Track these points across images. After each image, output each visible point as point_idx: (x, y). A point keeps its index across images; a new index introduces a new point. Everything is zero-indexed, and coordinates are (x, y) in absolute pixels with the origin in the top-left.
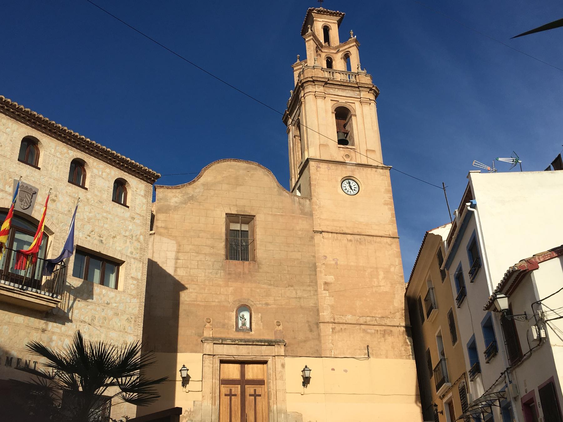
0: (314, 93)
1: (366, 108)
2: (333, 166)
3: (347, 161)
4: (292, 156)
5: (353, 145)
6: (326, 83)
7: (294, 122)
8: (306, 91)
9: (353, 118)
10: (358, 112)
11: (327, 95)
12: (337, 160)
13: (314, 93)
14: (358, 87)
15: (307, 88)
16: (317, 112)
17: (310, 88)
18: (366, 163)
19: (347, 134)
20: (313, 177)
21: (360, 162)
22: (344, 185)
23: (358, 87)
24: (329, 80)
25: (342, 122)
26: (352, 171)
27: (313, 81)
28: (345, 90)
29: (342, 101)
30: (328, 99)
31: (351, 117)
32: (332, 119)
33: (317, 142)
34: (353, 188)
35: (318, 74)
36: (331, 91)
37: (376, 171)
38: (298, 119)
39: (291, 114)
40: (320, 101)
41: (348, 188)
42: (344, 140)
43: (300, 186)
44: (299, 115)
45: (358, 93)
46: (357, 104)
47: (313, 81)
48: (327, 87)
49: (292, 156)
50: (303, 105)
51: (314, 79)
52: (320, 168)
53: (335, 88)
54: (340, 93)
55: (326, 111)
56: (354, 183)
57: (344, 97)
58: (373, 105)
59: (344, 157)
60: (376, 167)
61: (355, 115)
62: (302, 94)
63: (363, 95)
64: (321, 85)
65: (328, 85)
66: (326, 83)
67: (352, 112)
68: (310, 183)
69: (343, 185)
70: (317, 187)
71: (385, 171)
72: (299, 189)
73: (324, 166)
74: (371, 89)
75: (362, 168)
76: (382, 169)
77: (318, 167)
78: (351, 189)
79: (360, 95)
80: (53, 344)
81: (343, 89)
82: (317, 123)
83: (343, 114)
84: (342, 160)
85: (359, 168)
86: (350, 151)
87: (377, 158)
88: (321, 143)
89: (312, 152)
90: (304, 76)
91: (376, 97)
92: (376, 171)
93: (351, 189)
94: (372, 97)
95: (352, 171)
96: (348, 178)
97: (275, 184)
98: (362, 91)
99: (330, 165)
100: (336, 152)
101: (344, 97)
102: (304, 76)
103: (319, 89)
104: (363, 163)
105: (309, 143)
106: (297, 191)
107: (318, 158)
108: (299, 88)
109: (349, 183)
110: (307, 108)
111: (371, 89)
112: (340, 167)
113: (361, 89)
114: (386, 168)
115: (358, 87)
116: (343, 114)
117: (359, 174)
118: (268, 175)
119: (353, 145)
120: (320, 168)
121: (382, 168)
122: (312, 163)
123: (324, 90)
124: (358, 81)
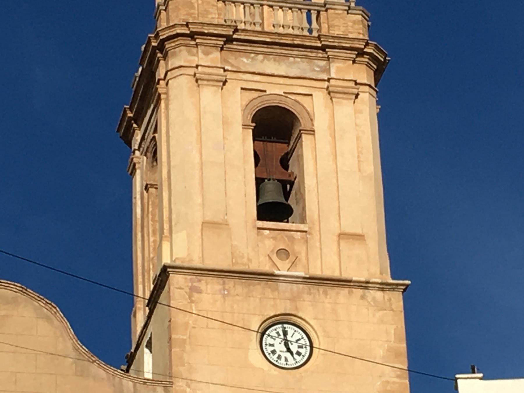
0: (191, 71)
1: (345, 108)
2: (237, 287)
3: (283, 268)
4: (139, 243)
5: (303, 220)
6: (229, 40)
7: (145, 145)
8: (173, 62)
9: (305, 138)
10: (320, 123)
11: (229, 75)
12: (254, 267)
13: (191, 71)
14: (323, 48)
15: (174, 54)
16: (200, 128)
17: (181, 56)
18: (336, 274)
19: (292, 184)
20: (179, 318)
21: (318, 273)
22: (270, 341)
23: (325, 48)
24: (236, 30)
25: (278, 149)
26: (293, 299)
27: (192, 36)
28: (287, 56)
29: (275, 91)
30: (234, 86)
31: (299, 137)
32: (242, 145)
33: (198, 217)
34: (294, 348)
35: (207, 12)
36: (245, 62)
37: (363, 297)
38: (154, 138)
39: (138, 119)
40: (209, 94)
41: (280, 347)
42: (277, 205)
43: (150, 338)
44: (155, 131)
45: (323, 63)
46: (319, 99)
47: (192, 36)
48: (231, 50)
49: (139, 243)
50: (163, 104)
51: (194, 28)
52: (200, 292)
53: (257, 53)
54: (270, 66)
55: (226, 123)
56: (299, 334)
57: (279, 79)
58: (367, 101)
59: (274, 257)
60: (365, 285)
61: (312, 132)
62: (161, 73)
63: (338, 70)
64: (215, 46)
65: (235, 46)
66: (229, 40)
67: (304, 123)
68: (170, 338)
69: (267, 340)
70: (188, 347)
71: (388, 294)
72: (149, 346)
73: (210, 287)
74: (361, 53)
75: (321, 289)
76: (382, 289)
77: (194, 290)
78: (289, 350)
79: (328, 71)
80: (232, 283)
81: (278, 55)
82: (197, 160)
83: (275, 129)
84: (266, 268)
85: (314, 289)
86: (292, 240)
87: (371, 260)
88: (207, 219)
89: (180, 247)
90: (168, 21)
91: (378, 74)
92: (363, 297)
93: (289, 350)
94: (363, 74)
95: (293, 299)
96: (283, 319)
97: (69, 344)
98: (336, 58)
99: (230, 283)
100: (252, 243)
101: (279, 79)
102: (168, 21)
103: (208, 58)
104: (327, 273)
105: (174, 216)
106: (146, 351)
107: (197, 263)
108: (154, 54)
109: (285, 333)
110: (173, 114)
111: (361, 53)
112: (258, 288)
113: (331, 52)
114: (392, 287)
115: (323, 48)
116: (275, 129)
117: (313, 308)
118: (48, 319)
119: (303, 220)
120: (200, 292)
121: (383, 287)
122: (176, 280)
123: (225, 60)
124: (324, 31)
